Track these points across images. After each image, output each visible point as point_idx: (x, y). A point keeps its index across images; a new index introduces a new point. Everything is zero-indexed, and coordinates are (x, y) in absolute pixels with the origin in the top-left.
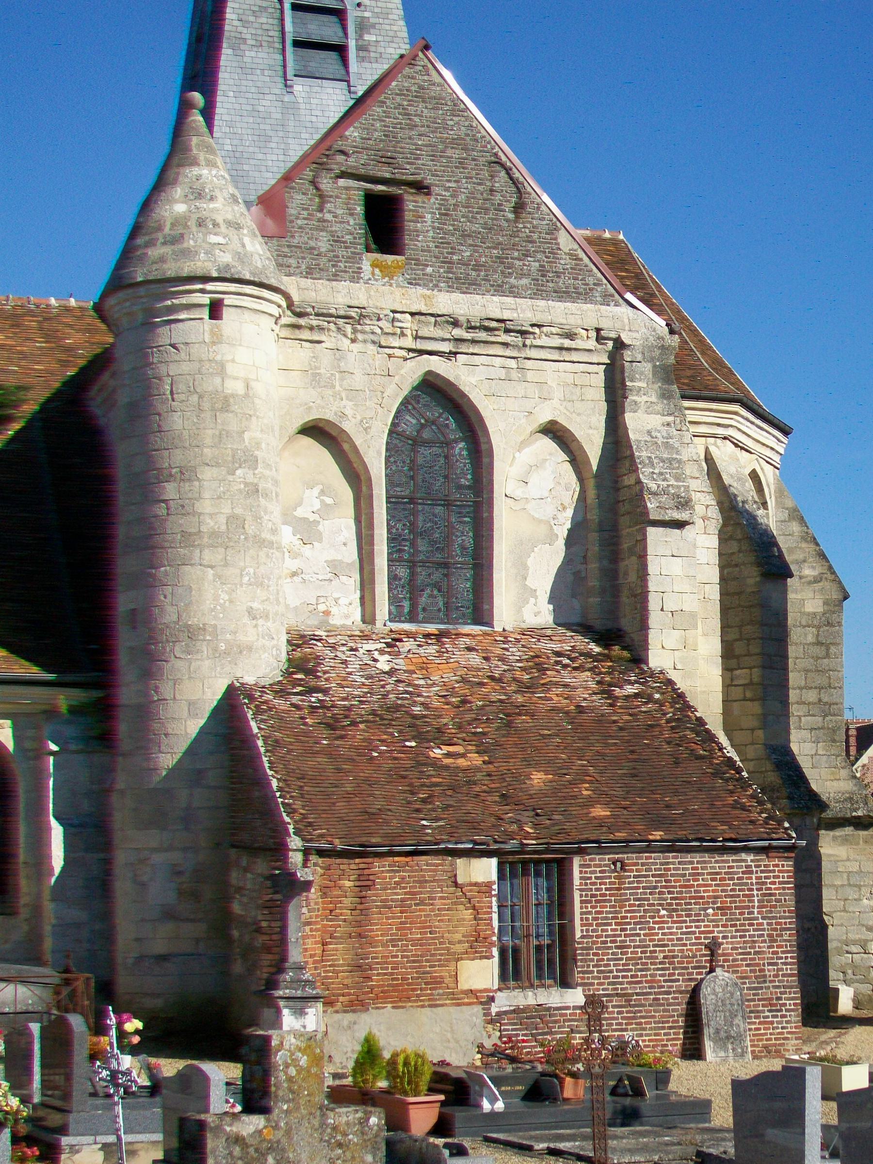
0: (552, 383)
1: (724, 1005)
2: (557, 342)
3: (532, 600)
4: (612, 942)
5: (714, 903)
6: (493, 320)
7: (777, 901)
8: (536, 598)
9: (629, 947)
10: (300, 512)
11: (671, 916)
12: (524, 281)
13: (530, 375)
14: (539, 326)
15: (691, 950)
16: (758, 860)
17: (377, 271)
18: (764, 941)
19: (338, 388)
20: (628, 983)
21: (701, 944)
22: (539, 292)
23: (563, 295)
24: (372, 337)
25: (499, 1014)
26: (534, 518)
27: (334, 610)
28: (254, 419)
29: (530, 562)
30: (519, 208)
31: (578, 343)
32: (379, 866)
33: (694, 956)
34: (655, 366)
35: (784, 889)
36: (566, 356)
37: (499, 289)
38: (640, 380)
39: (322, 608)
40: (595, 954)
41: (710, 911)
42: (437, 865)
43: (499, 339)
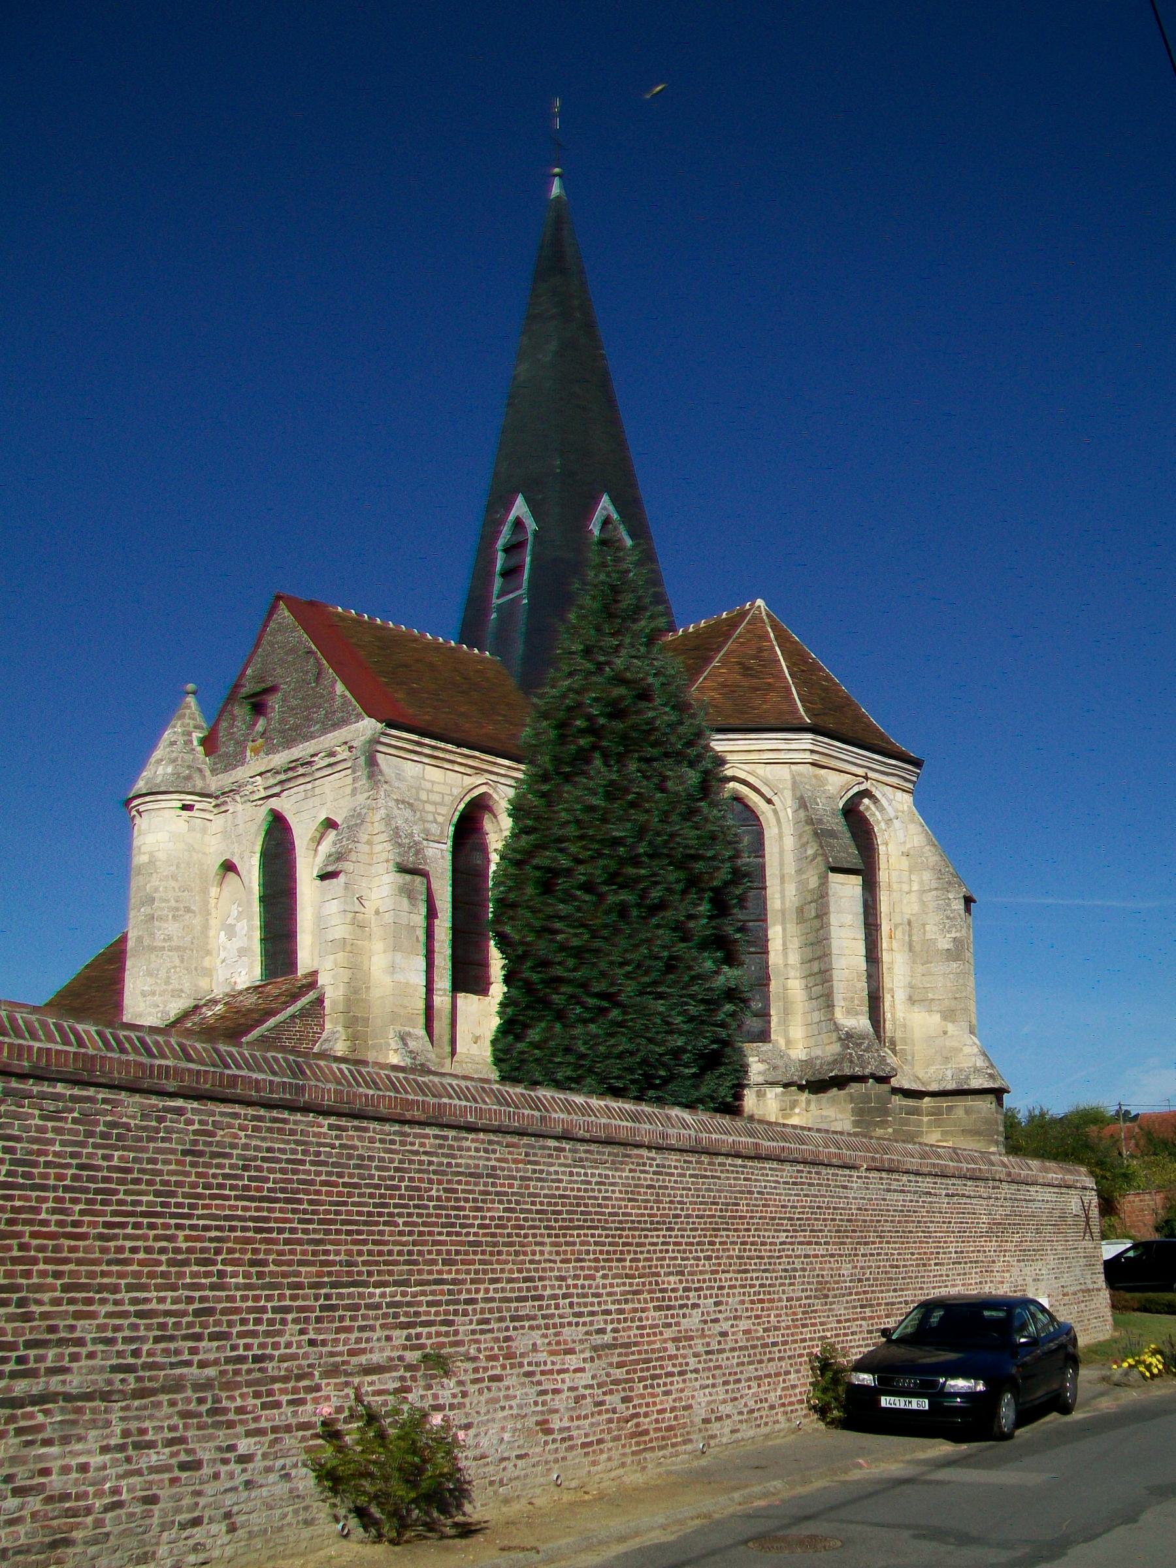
0: (327, 791)
13: (317, 791)
22: (324, 731)
23: (336, 726)
27: (238, 981)
28: (154, 875)
31: (339, 758)
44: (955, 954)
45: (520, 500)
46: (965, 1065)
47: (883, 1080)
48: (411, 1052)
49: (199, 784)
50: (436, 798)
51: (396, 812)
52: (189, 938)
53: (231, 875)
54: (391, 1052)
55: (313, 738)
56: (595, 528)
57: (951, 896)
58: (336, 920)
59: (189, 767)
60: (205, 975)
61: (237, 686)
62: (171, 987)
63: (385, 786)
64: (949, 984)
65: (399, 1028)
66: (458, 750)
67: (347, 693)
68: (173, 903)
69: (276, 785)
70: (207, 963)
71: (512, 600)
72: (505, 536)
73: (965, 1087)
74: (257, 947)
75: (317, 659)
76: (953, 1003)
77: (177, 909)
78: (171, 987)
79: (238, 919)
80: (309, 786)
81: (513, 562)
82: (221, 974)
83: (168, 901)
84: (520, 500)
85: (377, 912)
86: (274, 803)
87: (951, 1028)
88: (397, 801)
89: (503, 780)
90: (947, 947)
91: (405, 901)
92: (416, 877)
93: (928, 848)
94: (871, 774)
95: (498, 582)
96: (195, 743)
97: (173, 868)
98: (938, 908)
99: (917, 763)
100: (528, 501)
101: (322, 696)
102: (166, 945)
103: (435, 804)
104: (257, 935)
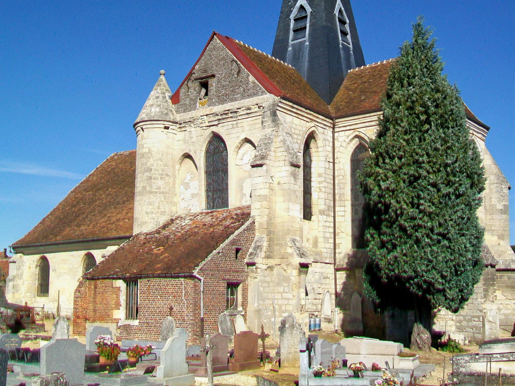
0: (246, 126)
1: (167, 328)
2: (246, 112)
3: (245, 197)
5: (172, 294)
6: (226, 111)
7: (190, 294)
11: (161, 298)
12: (239, 95)
13: (239, 125)
14: (240, 109)
15: (165, 310)
18: (185, 308)
19: (190, 142)
20: (150, 319)
22: (243, 97)
23: (250, 96)
24: (197, 125)
25: (120, 326)
26: (245, 170)
28: (151, 158)
30: (239, 71)
31: (252, 111)
32: (98, 282)
33: (166, 312)
34: (271, 112)
37: (232, 100)
39: (189, 208)
40: (143, 310)
41: (171, 297)
43: (229, 116)
44: (505, 211)
46: (508, 258)
47: (493, 266)
49: (172, 118)
50: (297, 132)
51: (287, 138)
52: (167, 188)
53: (188, 160)
54: (288, 248)
55: (237, 100)
56: (336, 12)
57: (503, 187)
59: (166, 109)
60: (174, 205)
61: (191, 74)
62: (160, 210)
63: (281, 126)
64: (501, 224)
66: (306, 111)
67: (256, 81)
68: (161, 172)
70: (175, 199)
71: (300, 42)
73: (509, 268)
75: (238, 64)
76: (503, 232)
77: (163, 175)
78: (160, 210)
80: (235, 122)
83: (158, 171)
85: (279, 183)
86: (214, 129)
87: (502, 242)
88: (286, 133)
89: (320, 125)
90: (501, 208)
91: (293, 179)
92: (296, 168)
93: (493, 165)
94: (475, 133)
96: (167, 98)
97: (160, 155)
98: (497, 191)
99: (488, 129)
102: (158, 191)
103: (297, 134)
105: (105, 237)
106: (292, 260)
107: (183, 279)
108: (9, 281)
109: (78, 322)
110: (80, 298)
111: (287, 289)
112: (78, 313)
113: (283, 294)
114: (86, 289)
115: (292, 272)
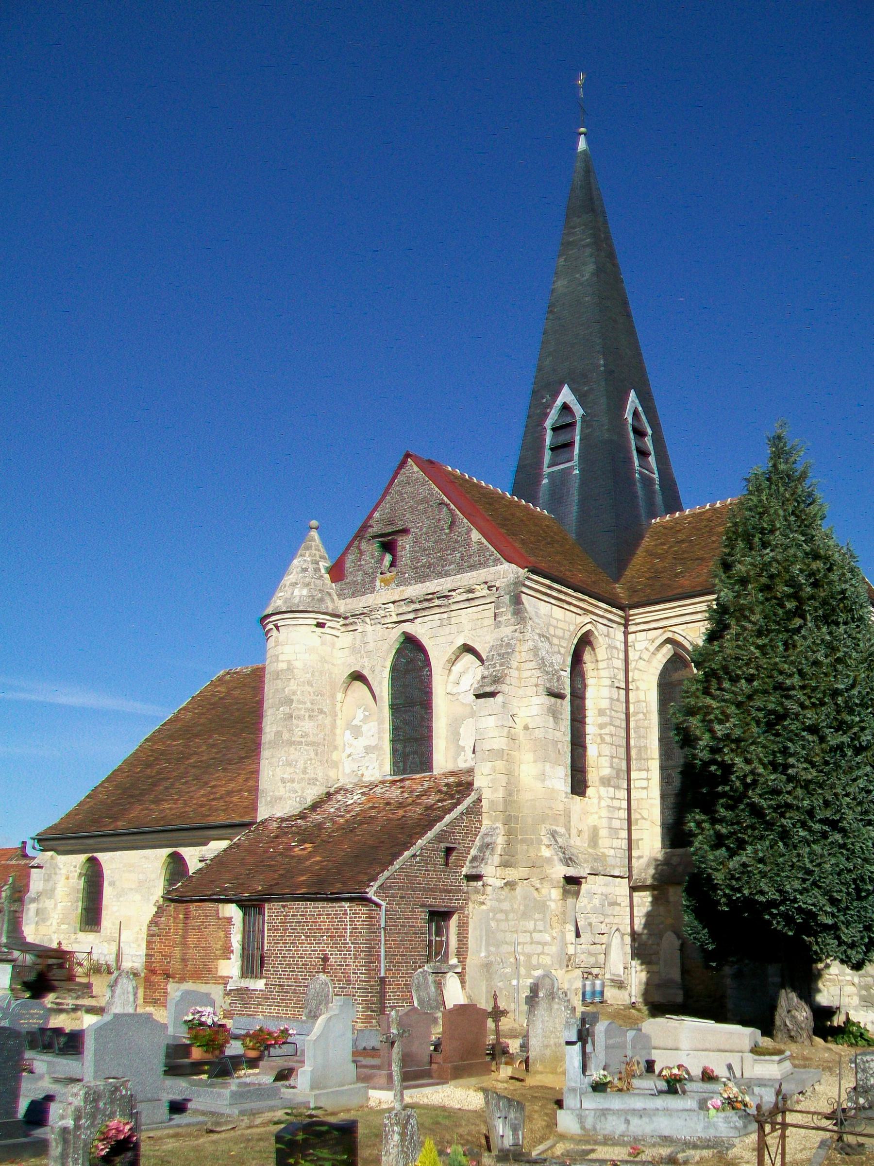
0: (465, 622)
3: (463, 753)
4: (281, 954)
5: (327, 933)
7: (360, 932)
8: (465, 751)
9: (287, 957)
10: (354, 723)
12: (453, 566)
13: (453, 620)
14: (454, 590)
16: (351, 907)
17: (383, 584)
18: (351, 958)
19: (362, 652)
21: (320, 958)
22: (460, 570)
23: (472, 567)
25: (231, 990)
26: (463, 704)
28: (292, 681)
29: (462, 731)
31: (477, 594)
32: (193, 907)
34: (511, 596)
35: (363, 925)
36: (473, 603)
37: (440, 575)
38: (503, 607)
39: (360, 773)
42: (212, 907)
43: (435, 604)
45: (566, 389)
48: (561, 847)
49: (330, 607)
50: (559, 633)
51: (540, 644)
52: (321, 736)
53: (358, 684)
54: (543, 847)
56: (628, 416)
58: (494, 733)
59: (321, 591)
62: (307, 776)
63: (531, 622)
65: (548, 826)
67: (484, 540)
68: (309, 705)
69: (409, 612)
70: (335, 756)
72: (552, 418)
74: (387, 746)
77: (313, 710)
79: (365, 720)
80: (445, 616)
81: (563, 438)
82: (348, 767)
83: (305, 703)
84: (566, 389)
85: (526, 728)
86: (408, 627)
88: (539, 634)
89: (600, 620)
95: (547, 456)
96: (323, 571)
97: (308, 676)
100: (573, 390)
101: (457, 542)
102: (303, 740)
103: (559, 638)
104: (387, 736)
105: (204, 822)
106: (551, 871)
107: (348, 904)
108: (30, 903)
109: (153, 982)
110: (158, 936)
111: (540, 925)
112: (154, 965)
113: (535, 934)
114: (170, 919)
115: (550, 894)
